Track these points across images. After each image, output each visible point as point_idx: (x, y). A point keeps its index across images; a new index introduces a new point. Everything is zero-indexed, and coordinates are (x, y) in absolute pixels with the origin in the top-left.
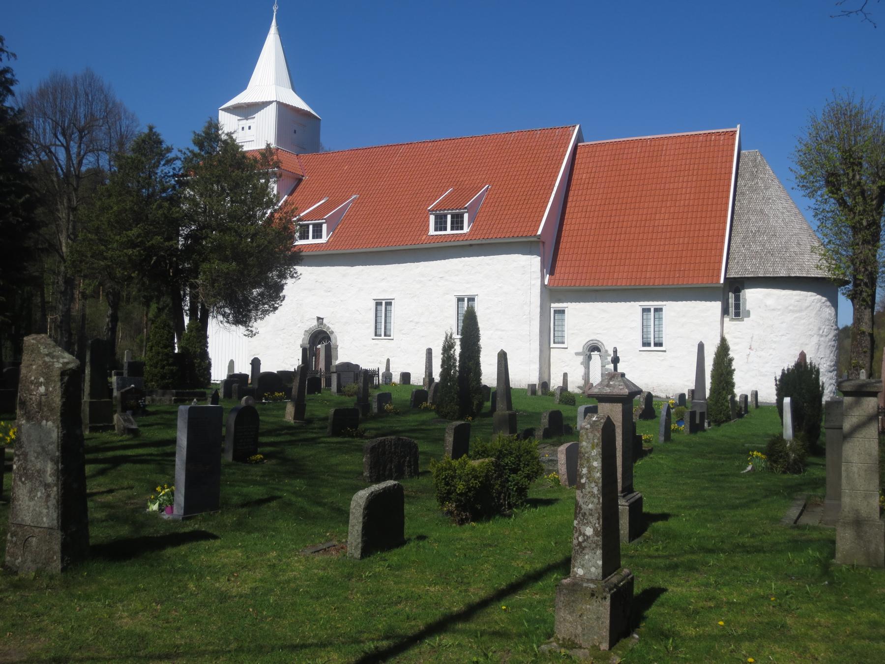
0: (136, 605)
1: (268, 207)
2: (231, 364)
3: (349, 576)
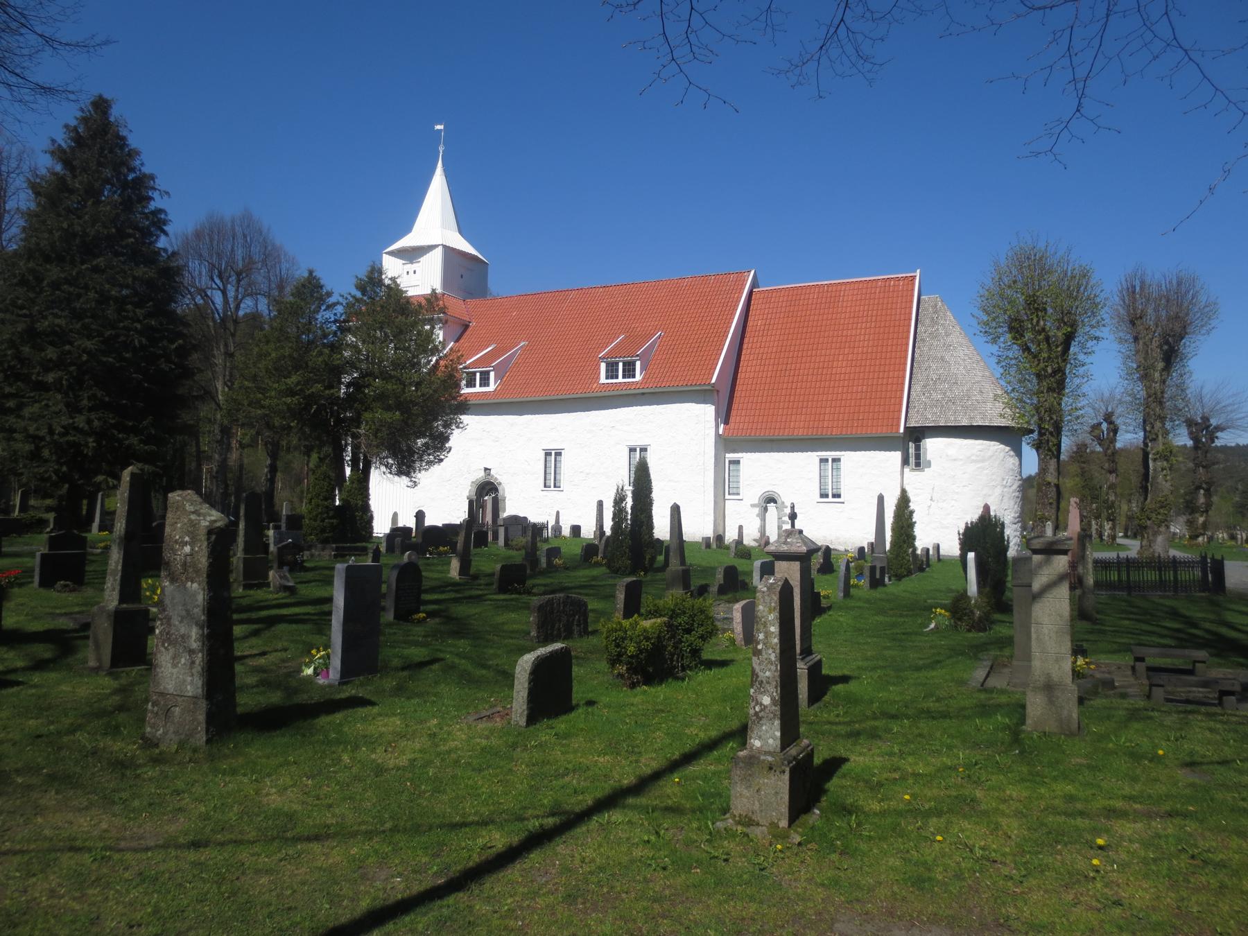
0: (285, 780)
1: (433, 355)
2: (395, 516)
3: (514, 746)
